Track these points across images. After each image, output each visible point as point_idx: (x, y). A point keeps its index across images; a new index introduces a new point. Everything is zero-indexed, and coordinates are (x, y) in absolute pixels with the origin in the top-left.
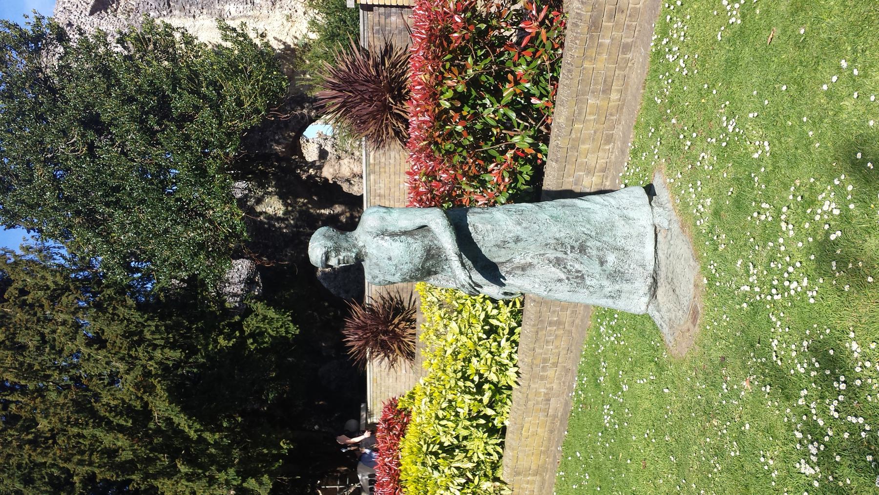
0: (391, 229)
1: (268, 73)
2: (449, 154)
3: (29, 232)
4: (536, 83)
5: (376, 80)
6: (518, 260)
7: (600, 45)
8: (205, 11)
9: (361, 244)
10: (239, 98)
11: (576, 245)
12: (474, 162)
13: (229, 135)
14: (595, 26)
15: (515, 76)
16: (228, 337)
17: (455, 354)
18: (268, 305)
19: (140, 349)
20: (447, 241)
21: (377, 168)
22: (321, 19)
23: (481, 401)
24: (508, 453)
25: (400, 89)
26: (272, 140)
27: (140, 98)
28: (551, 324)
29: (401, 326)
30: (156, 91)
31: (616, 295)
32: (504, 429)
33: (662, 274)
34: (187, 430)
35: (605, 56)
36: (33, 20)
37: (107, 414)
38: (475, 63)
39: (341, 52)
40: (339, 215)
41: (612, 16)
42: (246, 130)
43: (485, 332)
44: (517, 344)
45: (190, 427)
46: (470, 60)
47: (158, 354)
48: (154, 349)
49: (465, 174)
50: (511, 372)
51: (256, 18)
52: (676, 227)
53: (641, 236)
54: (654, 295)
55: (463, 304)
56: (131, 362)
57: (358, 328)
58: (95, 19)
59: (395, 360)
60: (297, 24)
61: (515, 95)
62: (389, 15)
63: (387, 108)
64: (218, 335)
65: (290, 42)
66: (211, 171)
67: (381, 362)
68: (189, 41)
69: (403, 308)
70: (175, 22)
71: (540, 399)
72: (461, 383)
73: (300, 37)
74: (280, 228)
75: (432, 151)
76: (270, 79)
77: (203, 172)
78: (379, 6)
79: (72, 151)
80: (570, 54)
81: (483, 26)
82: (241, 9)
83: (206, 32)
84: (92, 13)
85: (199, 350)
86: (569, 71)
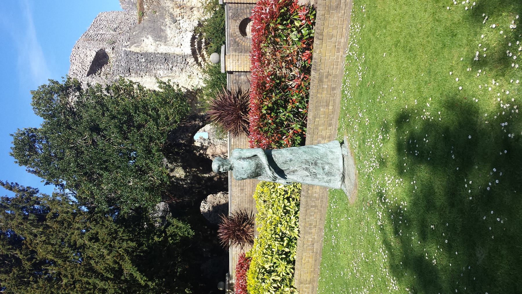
0: (243, 156)
1: (181, 103)
2: (266, 132)
3: (56, 186)
4: (300, 103)
5: (235, 105)
6: (291, 168)
7: (323, 88)
8: (147, 74)
9: (232, 163)
10: (166, 116)
11: (313, 162)
12: (277, 135)
13: (162, 134)
14: (321, 81)
15: (292, 100)
16: (159, 237)
17: (271, 223)
18: (179, 220)
19: (116, 242)
20: (264, 160)
21: (235, 147)
22: (208, 78)
23: (283, 245)
24: (297, 272)
25: (246, 109)
26: (179, 138)
27: (119, 116)
28: (312, 206)
29: (247, 227)
30: (126, 112)
31: (329, 181)
32: (294, 261)
33: (346, 173)
34: (140, 280)
35: (325, 92)
36: (66, 80)
37: (102, 271)
38: (276, 95)
39: (218, 93)
40: (213, 177)
41: (327, 77)
42: (170, 131)
43: (284, 213)
44: (298, 218)
45: (141, 279)
46: (274, 94)
47: (125, 244)
48: (123, 242)
49: (273, 140)
50: (296, 230)
51: (174, 77)
52: (349, 154)
53: (337, 159)
54: (343, 181)
55: (274, 201)
56: (110, 248)
57: (226, 228)
58: (89, 78)
59: (244, 245)
60: (193, 80)
61: (293, 108)
62: (240, 76)
63: (239, 117)
64: (154, 236)
65: (190, 88)
66: (153, 151)
67: (236, 247)
68: (141, 88)
69: (248, 218)
70: (134, 80)
71: (309, 244)
72: (273, 236)
73: (195, 86)
74: (182, 184)
75: (259, 131)
76: (182, 106)
77: (150, 152)
78: (236, 72)
79: (85, 143)
80: (312, 91)
81: (278, 81)
82: (166, 73)
83: (149, 83)
84: (88, 75)
85: (144, 244)
86: (312, 98)
